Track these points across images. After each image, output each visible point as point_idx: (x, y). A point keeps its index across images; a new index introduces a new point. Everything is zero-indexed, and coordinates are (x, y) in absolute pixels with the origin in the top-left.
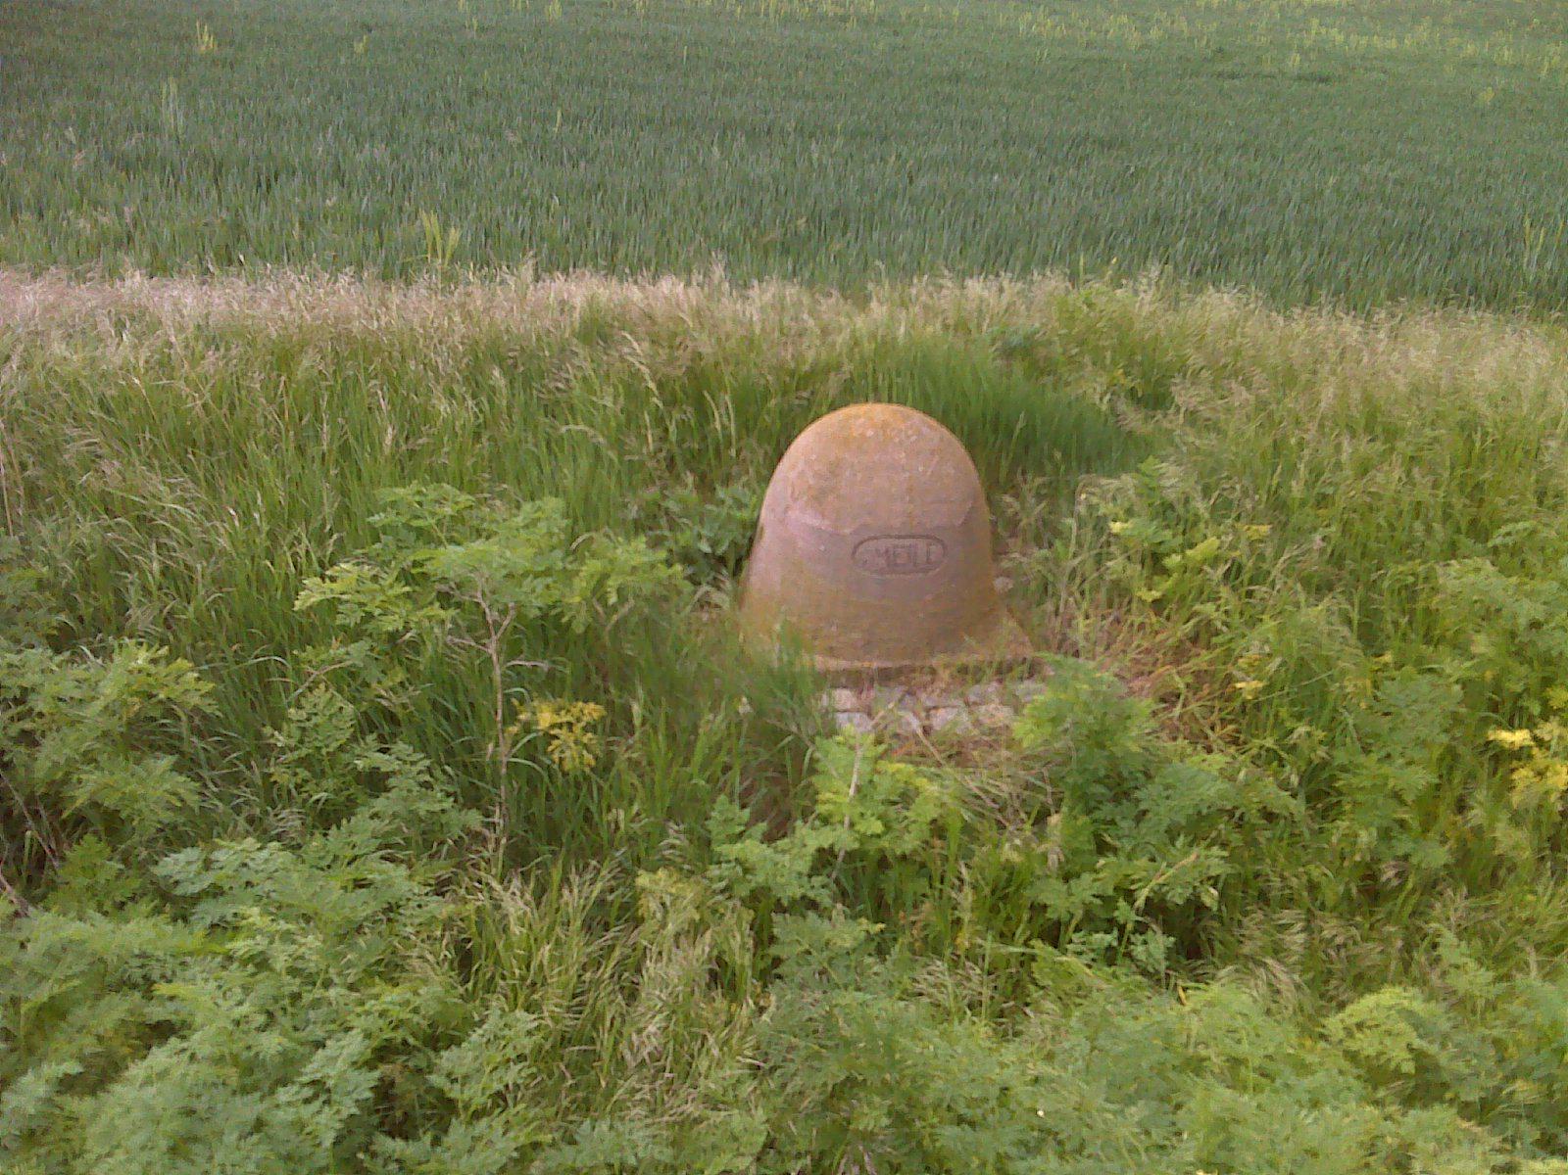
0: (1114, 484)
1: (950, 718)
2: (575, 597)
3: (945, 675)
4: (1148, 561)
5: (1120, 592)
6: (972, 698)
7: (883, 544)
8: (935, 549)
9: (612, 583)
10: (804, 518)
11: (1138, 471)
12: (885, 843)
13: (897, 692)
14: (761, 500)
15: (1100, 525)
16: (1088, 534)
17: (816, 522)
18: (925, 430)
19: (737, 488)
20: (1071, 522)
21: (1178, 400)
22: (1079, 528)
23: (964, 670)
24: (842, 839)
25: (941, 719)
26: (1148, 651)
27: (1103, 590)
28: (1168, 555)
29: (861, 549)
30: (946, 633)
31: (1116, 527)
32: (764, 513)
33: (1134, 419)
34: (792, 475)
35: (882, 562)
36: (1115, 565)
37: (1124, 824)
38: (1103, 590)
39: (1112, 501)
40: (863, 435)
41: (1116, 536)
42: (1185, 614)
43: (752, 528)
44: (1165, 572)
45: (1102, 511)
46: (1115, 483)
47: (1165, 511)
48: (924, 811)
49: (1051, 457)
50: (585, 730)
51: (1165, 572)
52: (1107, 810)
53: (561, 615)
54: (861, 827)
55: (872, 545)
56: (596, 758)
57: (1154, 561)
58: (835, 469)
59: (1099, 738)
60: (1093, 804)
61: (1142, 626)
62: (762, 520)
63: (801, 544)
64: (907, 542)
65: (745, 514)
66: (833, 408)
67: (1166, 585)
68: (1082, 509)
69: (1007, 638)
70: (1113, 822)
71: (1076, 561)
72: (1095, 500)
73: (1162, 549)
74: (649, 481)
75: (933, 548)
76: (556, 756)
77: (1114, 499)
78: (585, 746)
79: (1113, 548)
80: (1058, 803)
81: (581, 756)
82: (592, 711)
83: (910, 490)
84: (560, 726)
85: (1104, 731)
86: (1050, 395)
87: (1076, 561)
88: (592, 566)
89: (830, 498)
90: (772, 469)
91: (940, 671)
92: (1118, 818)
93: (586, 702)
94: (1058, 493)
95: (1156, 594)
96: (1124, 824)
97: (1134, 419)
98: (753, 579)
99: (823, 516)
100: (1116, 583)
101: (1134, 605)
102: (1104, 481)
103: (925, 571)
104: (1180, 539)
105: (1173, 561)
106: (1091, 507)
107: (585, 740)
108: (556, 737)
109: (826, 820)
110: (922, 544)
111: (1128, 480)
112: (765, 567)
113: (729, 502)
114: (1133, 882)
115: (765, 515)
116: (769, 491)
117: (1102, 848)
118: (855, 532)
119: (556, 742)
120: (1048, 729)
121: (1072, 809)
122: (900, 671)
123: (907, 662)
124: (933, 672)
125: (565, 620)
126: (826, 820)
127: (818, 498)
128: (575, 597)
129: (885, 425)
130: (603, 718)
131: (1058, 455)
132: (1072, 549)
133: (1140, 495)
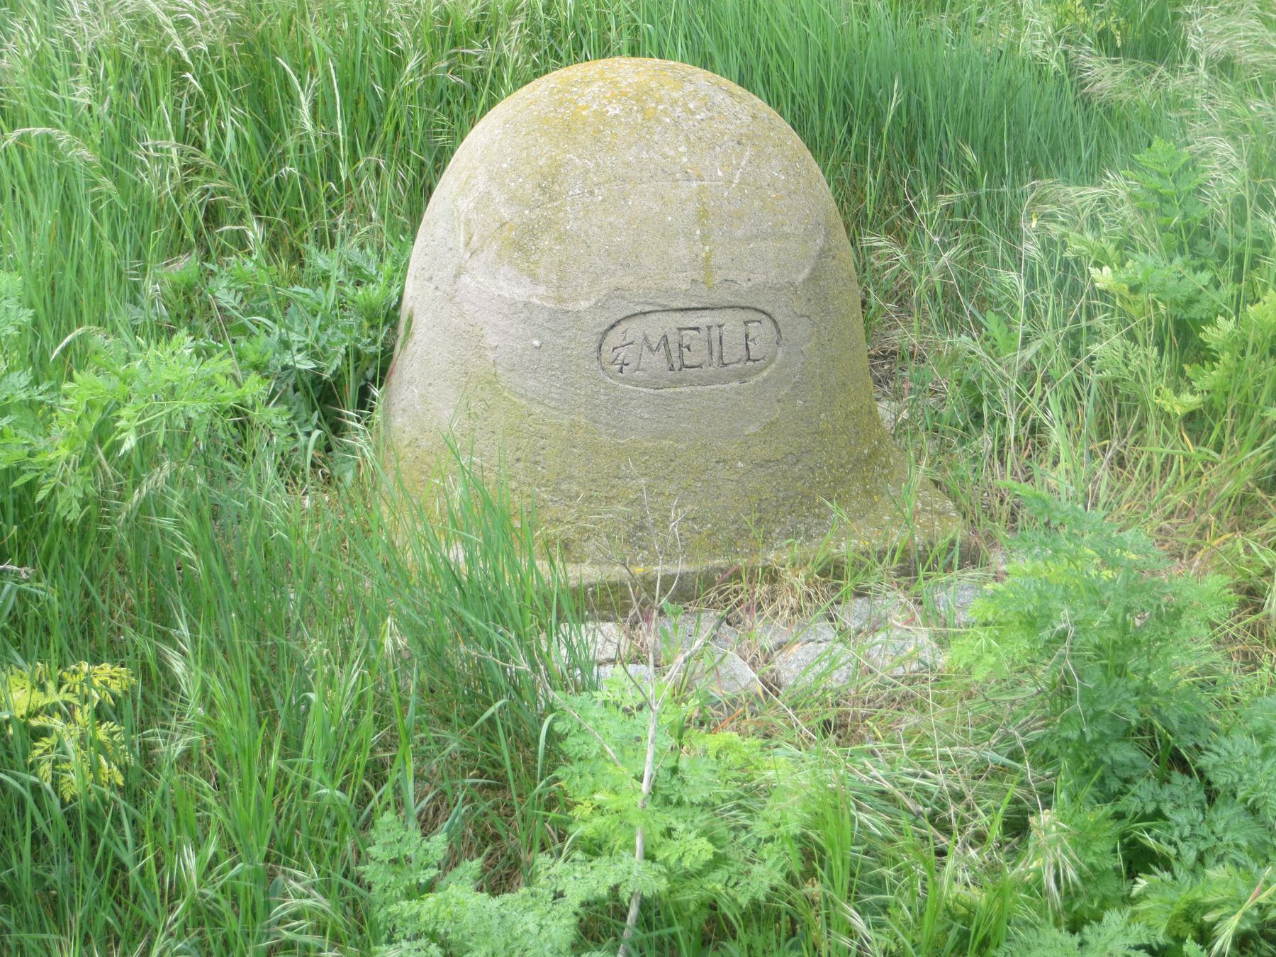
0: (1085, 195)
1: (810, 659)
2: (59, 449)
3: (797, 580)
4: (1171, 339)
5: (1118, 410)
6: (853, 625)
7: (657, 326)
8: (761, 331)
9: (128, 420)
10: (495, 287)
11: (1133, 165)
12: (715, 883)
13: (708, 621)
14: (401, 268)
15: (1070, 276)
16: (1047, 297)
17: (522, 291)
18: (720, 97)
19: (349, 249)
20: (1013, 279)
21: (1193, 42)
22: (1031, 285)
23: (832, 571)
24: (634, 876)
25: (795, 666)
26: (1185, 512)
27: (1088, 404)
28: (1209, 321)
29: (614, 338)
30: (794, 499)
31: (1104, 278)
32: (411, 287)
33: (1106, 77)
34: (465, 204)
35: (657, 361)
36: (1107, 348)
37: (1180, 817)
38: (1088, 404)
39: (1084, 220)
40: (601, 114)
41: (1104, 294)
42: (1254, 430)
43: (389, 316)
44: (1205, 356)
45: (1075, 247)
46: (1091, 193)
47: (1193, 239)
48: (787, 815)
49: (960, 159)
50: (100, 714)
51: (1205, 356)
52: (1142, 795)
53: (31, 487)
54: (668, 852)
55: (634, 329)
56: (124, 769)
57: (1183, 339)
58: (549, 184)
59: (1115, 656)
60: (1115, 785)
61: (1168, 462)
62: (407, 304)
63: (491, 340)
64: (704, 319)
65: (374, 293)
66: (521, 81)
67: (1208, 378)
68: (1030, 249)
69: (915, 507)
70: (1158, 814)
71: (1029, 353)
72: (1056, 230)
73: (1195, 312)
74: (175, 246)
75: (753, 329)
76: (45, 769)
77: (1094, 224)
78: (102, 748)
79: (1100, 319)
80: (1047, 796)
81: (95, 768)
82: (110, 678)
83: (702, 215)
84: (50, 711)
85: (1130, 643)
86: (946, 50)
87: (1029, 353)
88: (85, 387)
89: (546, 241)
90: (416, 216)
91: (788, 575)
92: (1167, 809)
93: (96, 661)
94: (984, 219)
95: (1190, 401)
96: (1180, 817)
97: (1106, 77)
98: (398, 421)
99: (535, 280)
100: (1111, 388)
101: (1151, 427)
102: (1072, 190)
103: (741, 377)
104: (1228, 290)
105: (1218, 333)
106: (1048, 246)
107: (101, 735)
108: (44, 732)
109: (594, 848)
110: (732, 323)
111: (1117, 184)
112: (421, 396)
113: (337, 274)
114: (1207, 908)
115: (416, 294)
116: (418, 254)
117: (1139, 859)
118: (601, 306)
119: (45, 743)
120: (1020, 645)
121: (1073, 798)
122: (708, 581)
123: (720, 562)
124: (773, 577)
125: (41, 495)
126: (594, 848)
127: (520, 245)
128: (59, 449)
129: (641, 95)
130: (129, 693)
131: (971, 156)
132: (1021, 329)
133: (1143, 211)
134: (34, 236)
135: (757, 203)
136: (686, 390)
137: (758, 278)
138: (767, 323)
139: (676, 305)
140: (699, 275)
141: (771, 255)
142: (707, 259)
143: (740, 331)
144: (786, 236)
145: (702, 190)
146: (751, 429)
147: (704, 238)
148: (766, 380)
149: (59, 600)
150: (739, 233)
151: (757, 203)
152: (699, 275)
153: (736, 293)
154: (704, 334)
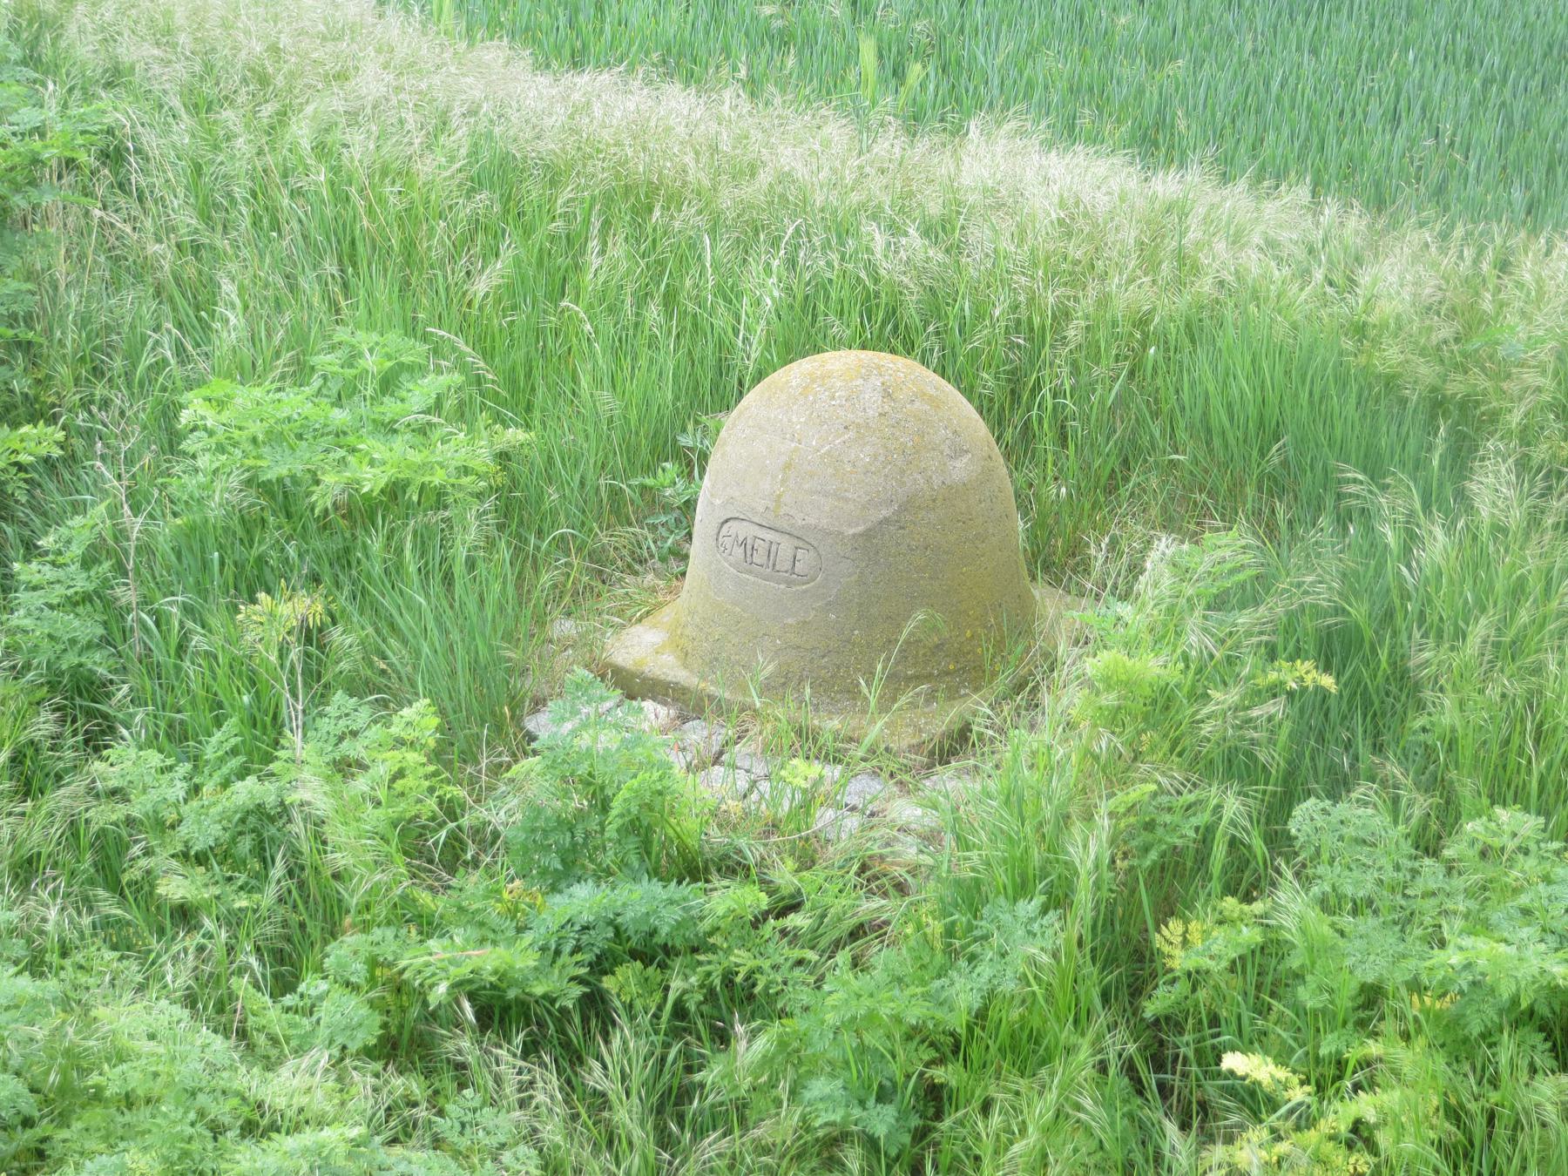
83: (788, 466)
134: (653, 712)
135: (830, 471)
136: (752, 578)
137: (812, 521)
138: (812, 553)
139: (756, 520)
140: (772, 505)
141: (827, 509)
142: (779, 496)
143: (790, 553)
144: (846, 500)
145: (796, 450)
146: (790, 621)
147: (783, 481)
148: (805, 592)
149: (650, 210)
150: (806, 486)
151: (830, 471)
152: (772, 505)
153: (792, 526)
154: (766, 545)
